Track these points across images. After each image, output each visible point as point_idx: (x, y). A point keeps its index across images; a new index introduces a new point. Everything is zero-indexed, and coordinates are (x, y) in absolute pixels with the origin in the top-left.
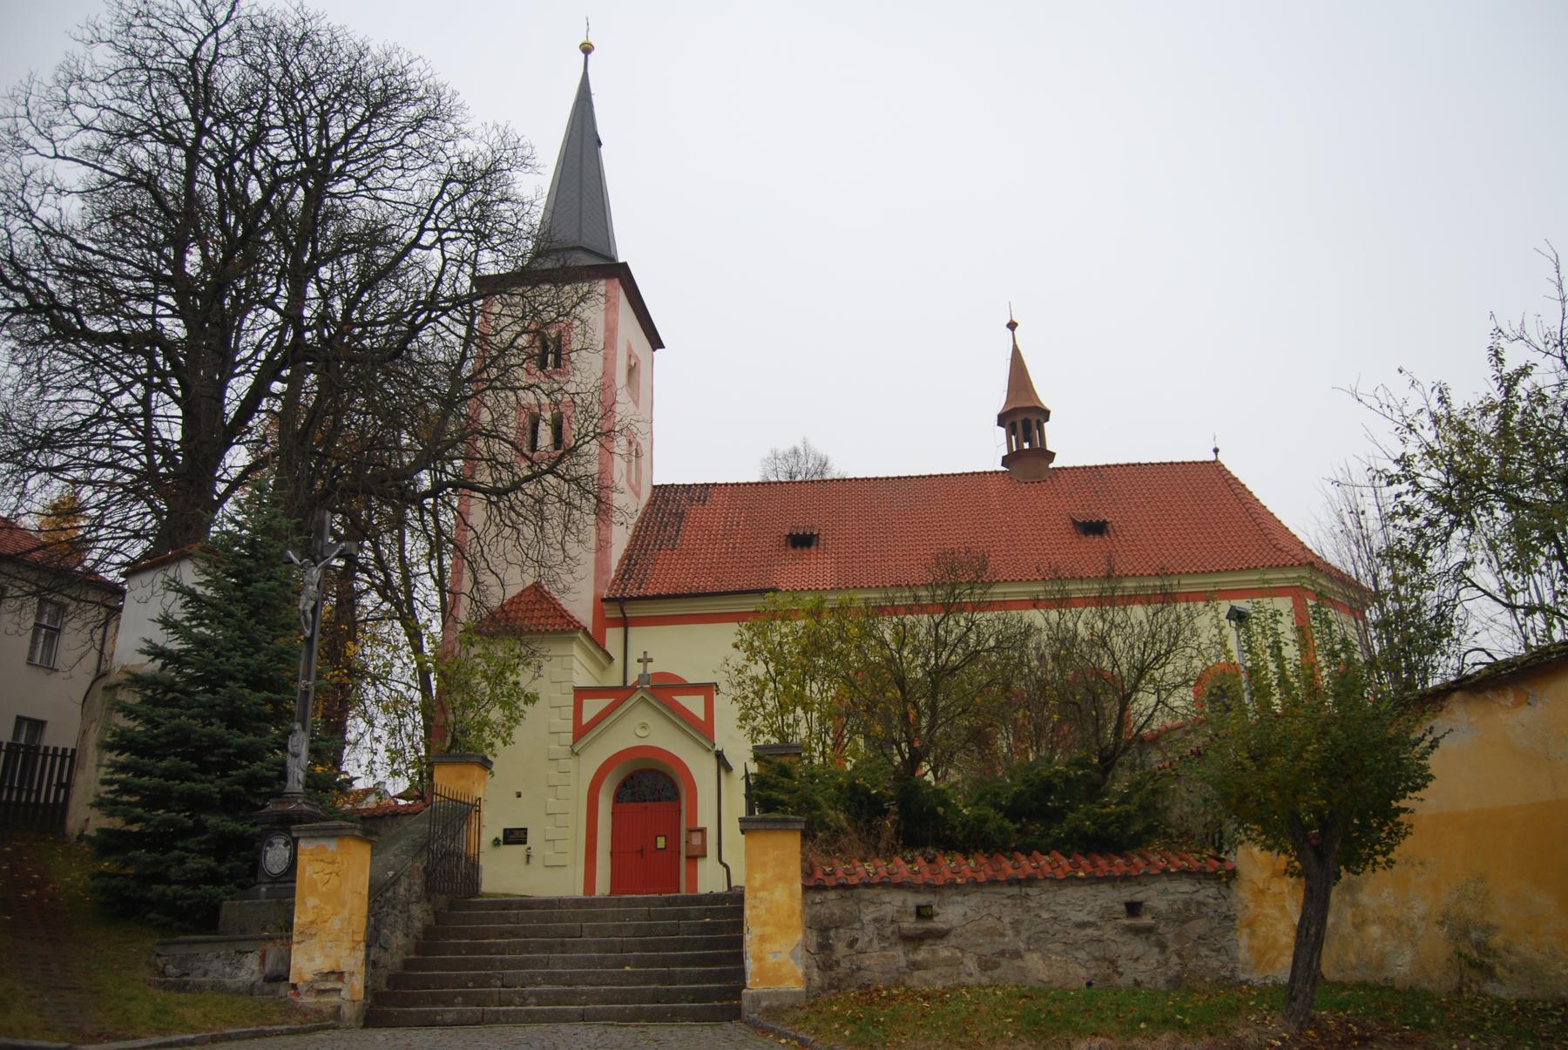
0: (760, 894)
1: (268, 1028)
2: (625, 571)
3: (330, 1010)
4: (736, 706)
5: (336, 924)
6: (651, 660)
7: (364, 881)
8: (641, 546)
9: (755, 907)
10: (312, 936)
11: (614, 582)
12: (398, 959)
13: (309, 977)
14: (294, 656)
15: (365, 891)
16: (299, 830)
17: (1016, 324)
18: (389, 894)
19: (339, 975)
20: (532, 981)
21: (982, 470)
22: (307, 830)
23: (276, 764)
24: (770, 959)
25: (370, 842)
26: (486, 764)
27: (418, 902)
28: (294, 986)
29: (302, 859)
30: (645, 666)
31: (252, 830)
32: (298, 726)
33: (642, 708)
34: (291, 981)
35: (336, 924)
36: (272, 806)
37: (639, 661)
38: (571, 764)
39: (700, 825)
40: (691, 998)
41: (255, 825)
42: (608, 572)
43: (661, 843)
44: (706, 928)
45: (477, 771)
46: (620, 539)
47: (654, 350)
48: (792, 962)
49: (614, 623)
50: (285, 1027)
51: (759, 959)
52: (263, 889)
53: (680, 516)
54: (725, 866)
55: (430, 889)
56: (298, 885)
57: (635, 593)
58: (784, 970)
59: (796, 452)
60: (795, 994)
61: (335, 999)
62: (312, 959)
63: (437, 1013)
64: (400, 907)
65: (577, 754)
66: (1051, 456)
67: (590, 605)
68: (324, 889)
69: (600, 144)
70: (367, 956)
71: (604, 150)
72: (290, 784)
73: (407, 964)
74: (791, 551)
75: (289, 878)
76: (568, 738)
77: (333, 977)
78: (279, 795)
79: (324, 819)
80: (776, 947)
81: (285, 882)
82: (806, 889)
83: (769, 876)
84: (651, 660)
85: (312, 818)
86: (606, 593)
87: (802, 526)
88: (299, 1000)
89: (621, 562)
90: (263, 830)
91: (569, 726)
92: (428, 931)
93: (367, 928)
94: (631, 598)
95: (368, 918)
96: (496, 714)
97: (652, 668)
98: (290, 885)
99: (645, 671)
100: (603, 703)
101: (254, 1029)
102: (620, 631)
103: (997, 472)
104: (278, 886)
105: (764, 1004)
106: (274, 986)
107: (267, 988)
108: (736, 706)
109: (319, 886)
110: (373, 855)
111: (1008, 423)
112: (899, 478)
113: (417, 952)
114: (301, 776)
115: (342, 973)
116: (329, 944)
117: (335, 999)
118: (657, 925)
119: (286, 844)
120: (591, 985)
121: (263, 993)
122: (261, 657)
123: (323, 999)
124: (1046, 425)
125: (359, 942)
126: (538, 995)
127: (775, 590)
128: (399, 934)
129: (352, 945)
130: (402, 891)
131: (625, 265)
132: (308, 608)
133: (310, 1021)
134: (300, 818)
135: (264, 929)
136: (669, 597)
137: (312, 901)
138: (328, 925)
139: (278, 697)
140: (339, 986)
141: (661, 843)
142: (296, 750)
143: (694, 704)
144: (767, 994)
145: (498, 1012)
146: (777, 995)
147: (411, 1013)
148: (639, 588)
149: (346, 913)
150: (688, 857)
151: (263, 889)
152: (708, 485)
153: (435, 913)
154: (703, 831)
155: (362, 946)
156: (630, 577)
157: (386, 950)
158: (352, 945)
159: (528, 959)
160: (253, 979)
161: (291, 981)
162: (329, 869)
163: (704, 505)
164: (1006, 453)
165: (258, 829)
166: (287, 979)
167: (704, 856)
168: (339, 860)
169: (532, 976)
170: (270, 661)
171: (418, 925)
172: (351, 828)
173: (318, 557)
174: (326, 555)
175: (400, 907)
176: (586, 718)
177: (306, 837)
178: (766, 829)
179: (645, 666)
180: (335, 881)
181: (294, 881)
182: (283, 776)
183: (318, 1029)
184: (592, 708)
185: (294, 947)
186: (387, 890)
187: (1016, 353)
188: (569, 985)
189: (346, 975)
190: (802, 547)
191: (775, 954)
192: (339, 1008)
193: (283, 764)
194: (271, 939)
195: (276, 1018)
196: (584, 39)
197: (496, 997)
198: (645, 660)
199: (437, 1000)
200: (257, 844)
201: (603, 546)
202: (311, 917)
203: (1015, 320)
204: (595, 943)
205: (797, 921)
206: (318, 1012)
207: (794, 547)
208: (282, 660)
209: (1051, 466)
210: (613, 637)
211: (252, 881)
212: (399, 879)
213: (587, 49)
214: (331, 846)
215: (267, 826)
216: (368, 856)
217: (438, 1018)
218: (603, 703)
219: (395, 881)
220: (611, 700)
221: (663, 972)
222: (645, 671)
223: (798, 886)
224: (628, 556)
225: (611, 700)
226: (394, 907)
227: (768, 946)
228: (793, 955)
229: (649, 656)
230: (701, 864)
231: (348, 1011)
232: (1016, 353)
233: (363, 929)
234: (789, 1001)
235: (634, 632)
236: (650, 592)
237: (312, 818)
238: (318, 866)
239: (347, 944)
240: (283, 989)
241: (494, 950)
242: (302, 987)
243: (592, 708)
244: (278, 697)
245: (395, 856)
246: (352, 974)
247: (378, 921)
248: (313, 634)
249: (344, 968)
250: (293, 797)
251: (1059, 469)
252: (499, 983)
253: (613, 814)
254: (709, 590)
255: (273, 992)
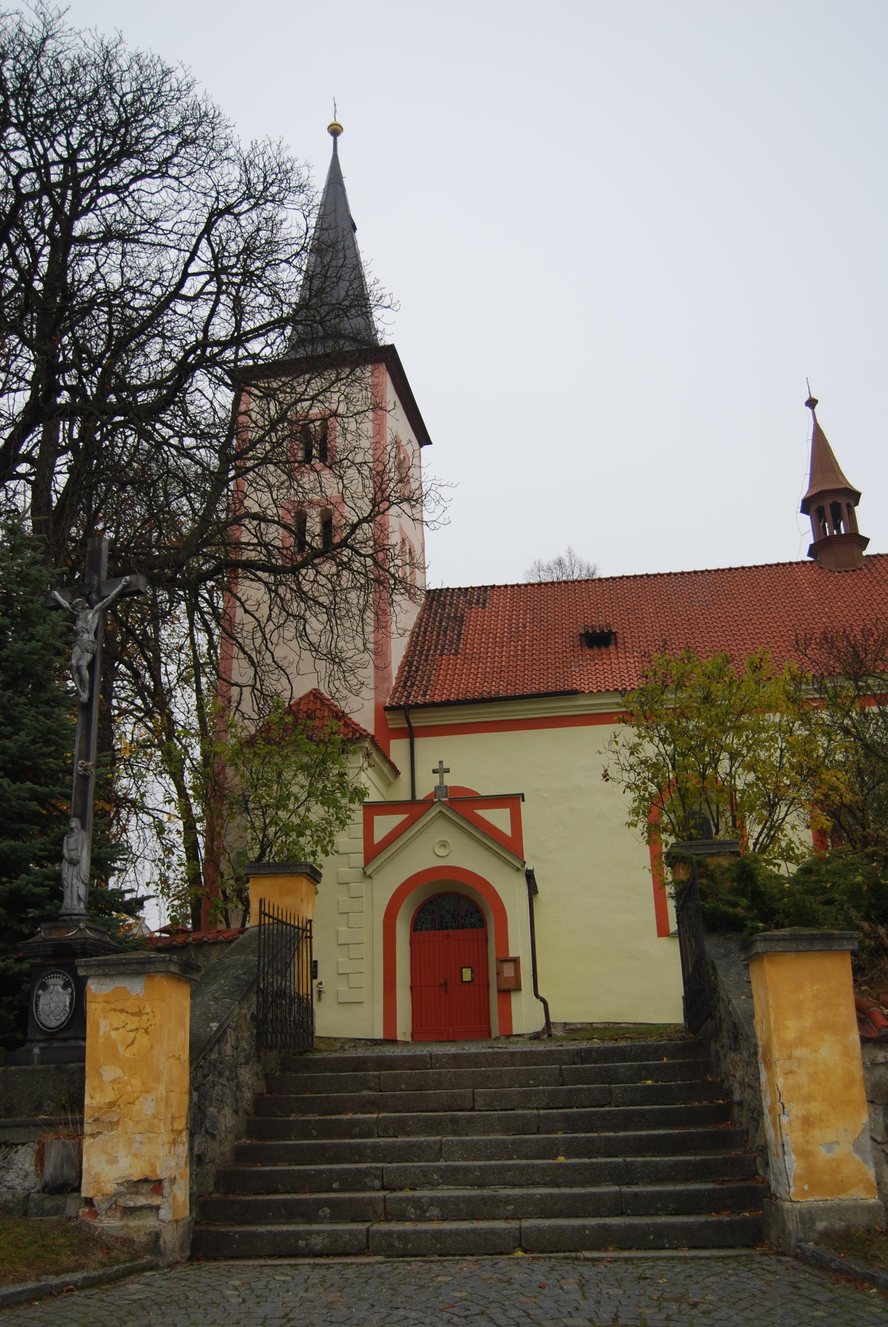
0: (798, 1052)
1: (53, 1280)
2: (407, 679)
3: (144, 1239)
4: (631, 795)
5: (147, 1107)
6: (447, 771)
7: (183, 1038)
8: (421, 652)
9: (791, 1072)
10: (113, 1125)
11: (395, 690)
12: (227, 1148)
13: (110, 1188)
14: (65, 738)
15: (185, 1055)
16: (87, 966)
17: (816, 402)
18: (214, 1056)
19: (156, 1185)
20: (424, 1180)
21: (787, 561)
22: (100, 965)
23: (47, 877)
24: (822, 1155)
25: (190, 980)
26: (314, 876)
27: (247, 1063)
28: (89, 1202)
29: (94, 1009)
30: (442, 778)
31: (17, 968)
32: (75, 823)
33: (441, 824)
34: (83, 1195)
35: (147, 1107)
36: (43, 933)
37: (435, 772)
38: (363, 888)
39: (512, 954)
40: (672, 1206)
41: (20, 960)
42: (388, 678)
43: (467, 975)
44: (650, 1095)
45: (304, 885)
46: (398, 649)
47: (421, 446)
48: (858, 1158)
49: (398, 734)
50: (79, 1276)
51: (805, 1154)
52: (37, 1051)
53: (460, 620)
54: (543, 1000)
55: (261, 1042)
56: (89, 1043)
57: (420, 700)
58: (846, 1171)
59: (560, 563)
60: (869, 1209)
61: (150, 1222)
62: (113, 1161)
63: (298, 1235)
64: (227, 1073)
65: (370, 877)
66: (865, 541)
67: (372, 716)
68: (128, 1054)
69: (354, 228)
70: (191, 1149)
71: (358, 235)
72: (67, 901)
73: (240, 1154)
74: (588, 651)
75: (71, 1034)
76: (359, 859)
77: (146, 1188)
78: (55, 918)
79: (115, 951)
80: (829, 1135)
81: (65, 1040)
82: (864, 1041)
83: (808, 1023)
84: (447, 771)
85: (99, 948)
86: (387, 702)
87: (597, 621)
88: (96, 1223)
89: (401, 669)
90: (33, 966)
91: (360, 845)
92: (259, 1102)
93: (190, 1108)
94: (417, 706)
95: (191, 1094)
96: (317, 812)
97: (450, 781)
98: (81, 1043)
99: (442, 782)
100: (396, 820)
101: (31, 1285)
102: (404, 743)
103: (804, 563)
104: (56, 1044)
105: (821, 1225)
106: (58, 1200)
107: (48, 1203)
108: (631, 795)
109: (121, 1049)
110: (193, 996)
111: (814, 508)
112: (695, 572)
113: (250, 1134)
114: (82, 891)
115: (160, 1181)
116: (139, 1138)
117: (150, 1222)
118: (580, 1090)
119: (65, 986)
120: (514, 1186)
121: (43, 1212)
122: (22, 736)
123: (134, 1223)
124: (856, 508)
125: (180, 1132)
126: (441, 1203)
127: (574, 693)
128: (227, 1111)
129: (173, 1136)
130: (228, 1049)
131: (391, 350)
132: (84, 663)
133: (118, 1261)
134: (87, 949)
135: (39, 1108)
136: (458, 703)
137: (110, 1073)
138: (136, 1107)
139: (45, 790)
140: (156, 1201)
141: (467, 975)
142: (73, 854)
143: (499, 819)
144: (823, 1210)
145: (390, 1233)
146: (840, 1210)
147: (260, 1235)
148: (424, 695)
149: (162, 1090)
150: (500, 991)
151: (37, 1051)
152: (486, 587)
153: (266, 1076)
154: (516, 961)
155: (185, 1137)
156: (413, 684)
157: (213, 1136)
158: (173, 1136)
159: (412, 1145)
160: (27, 1185)
161: (83, 1195)
162: (134, 1022)
163: (484, 607)
164: (812, 542)
165: (26, 965)
166: (78, 1189)
167: (519, 989)
168: (148, 1009)
169: (425, 1172)
170: (33, 742)
171: (248, 1094)
172: (164, 960)
173: (94, 597)
174: (104, 593)
175: (227, 1073)
176: (379, 835)
177: (96, 976)
178: (798, 951)
179: (442, 778)
180: (143, 1040)
181: (84, 1039)
182: (57, 894)
183: (129, 1272)
184: (384, 825)
185: (87, 1142)
186: (211, 1050)
187: (818, 435)
188: (481, 1186)
189: (166, 1184)
190: (599, 646)
191: (829, 1147)
192: (157, 1236)
193: (58, 878)
194: (49, 1124)
195: (66, 1259)
196: (332, 121)
197: (380, 1209)
198: (441, 770)
199: (292, 1212)
200: (25, 986)
201: (381, 653)
202: (109, 1096)
203: (814, 396)
204: (499, 1119)
205: (858, 1093)
206: (127, 1242)
207: (591, 646)
208: (48, 742)
209: (865, 553)
210: (398, 749)
211: (20, 1036)
212: (225, 1033)
213: (335, 131)
214: (136, 987)
215: (39, 960)
216: (187, 1003)
217: (301, 1243)
218: (396, 820)
219: (220, 1038)
220: (405, 816)
221: (617, 1165)
222: (442, 782)
223: (855, 1037)
224: (408, 663)
225: (405, 816)
226: (220, 1075)
227: (816, 1133)
228: (857, 1147)
229: (445, 766)
230: (515, 998)
231: (171, 1238)
232: (818, 435)
233: (184, 1110)
234: (861, 1220)
235: (421, 743)
236: (437, 698)
237: (99, 948)
238: (117, 1019)
239: (166, 1137)
240: (71, 1206)
241: (356, 1130)
242: (101, 1204)
243: (384, 825)
244: (45, 790)
245: (216, 1000)
246: (173, 1181)
247: (202, 1096)
248: (91, 698)
249: (162, 1174)
250: (71, 920)
251: (874, 556)
252: (377, 1183)
253: (411, 944)
254: (502, 694)
255: (58, 1210)
